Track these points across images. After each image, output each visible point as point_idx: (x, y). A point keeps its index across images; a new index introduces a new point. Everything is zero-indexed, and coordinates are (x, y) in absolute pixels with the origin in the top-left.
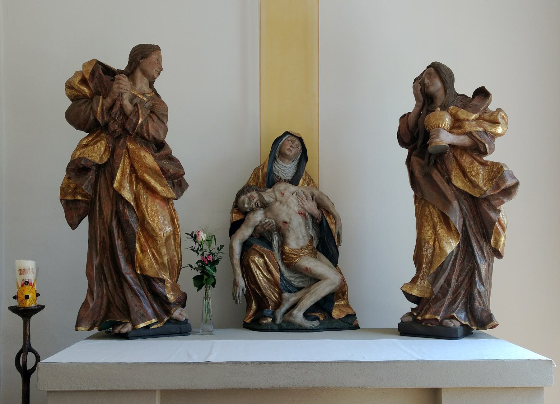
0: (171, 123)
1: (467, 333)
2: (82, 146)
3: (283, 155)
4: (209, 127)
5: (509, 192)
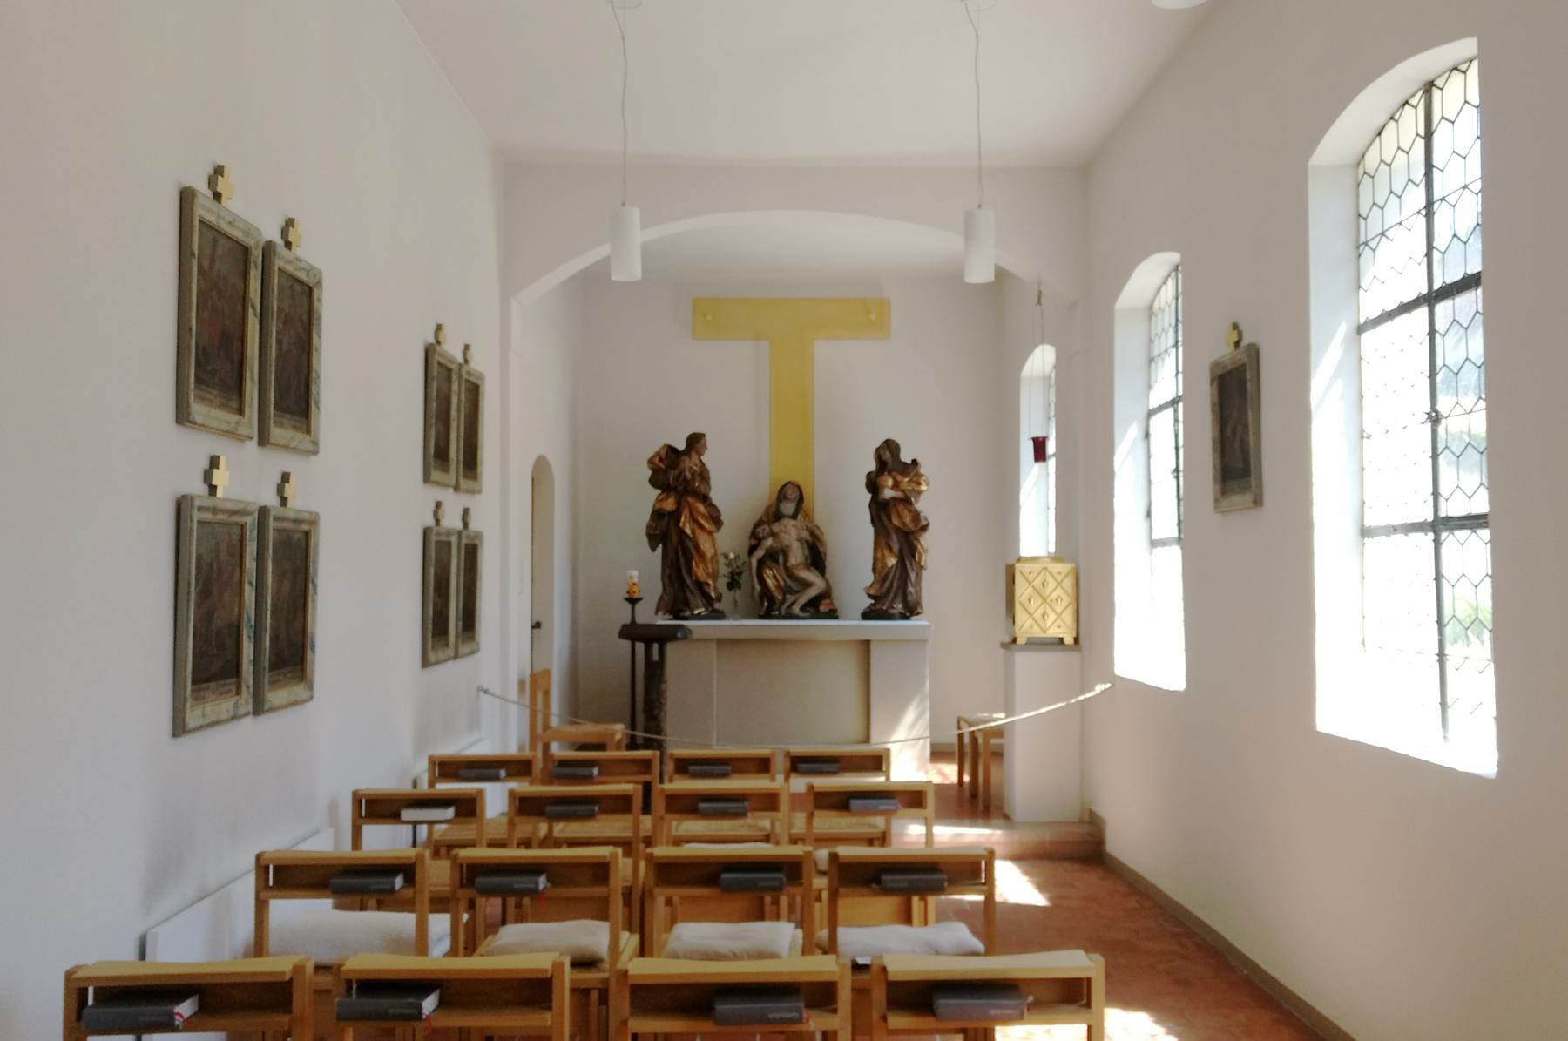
0: (713, 482)
1: (904, 617)
2: (658, 500)
3: (786, 498)
4: (736, 486)
5: (924, 528)
